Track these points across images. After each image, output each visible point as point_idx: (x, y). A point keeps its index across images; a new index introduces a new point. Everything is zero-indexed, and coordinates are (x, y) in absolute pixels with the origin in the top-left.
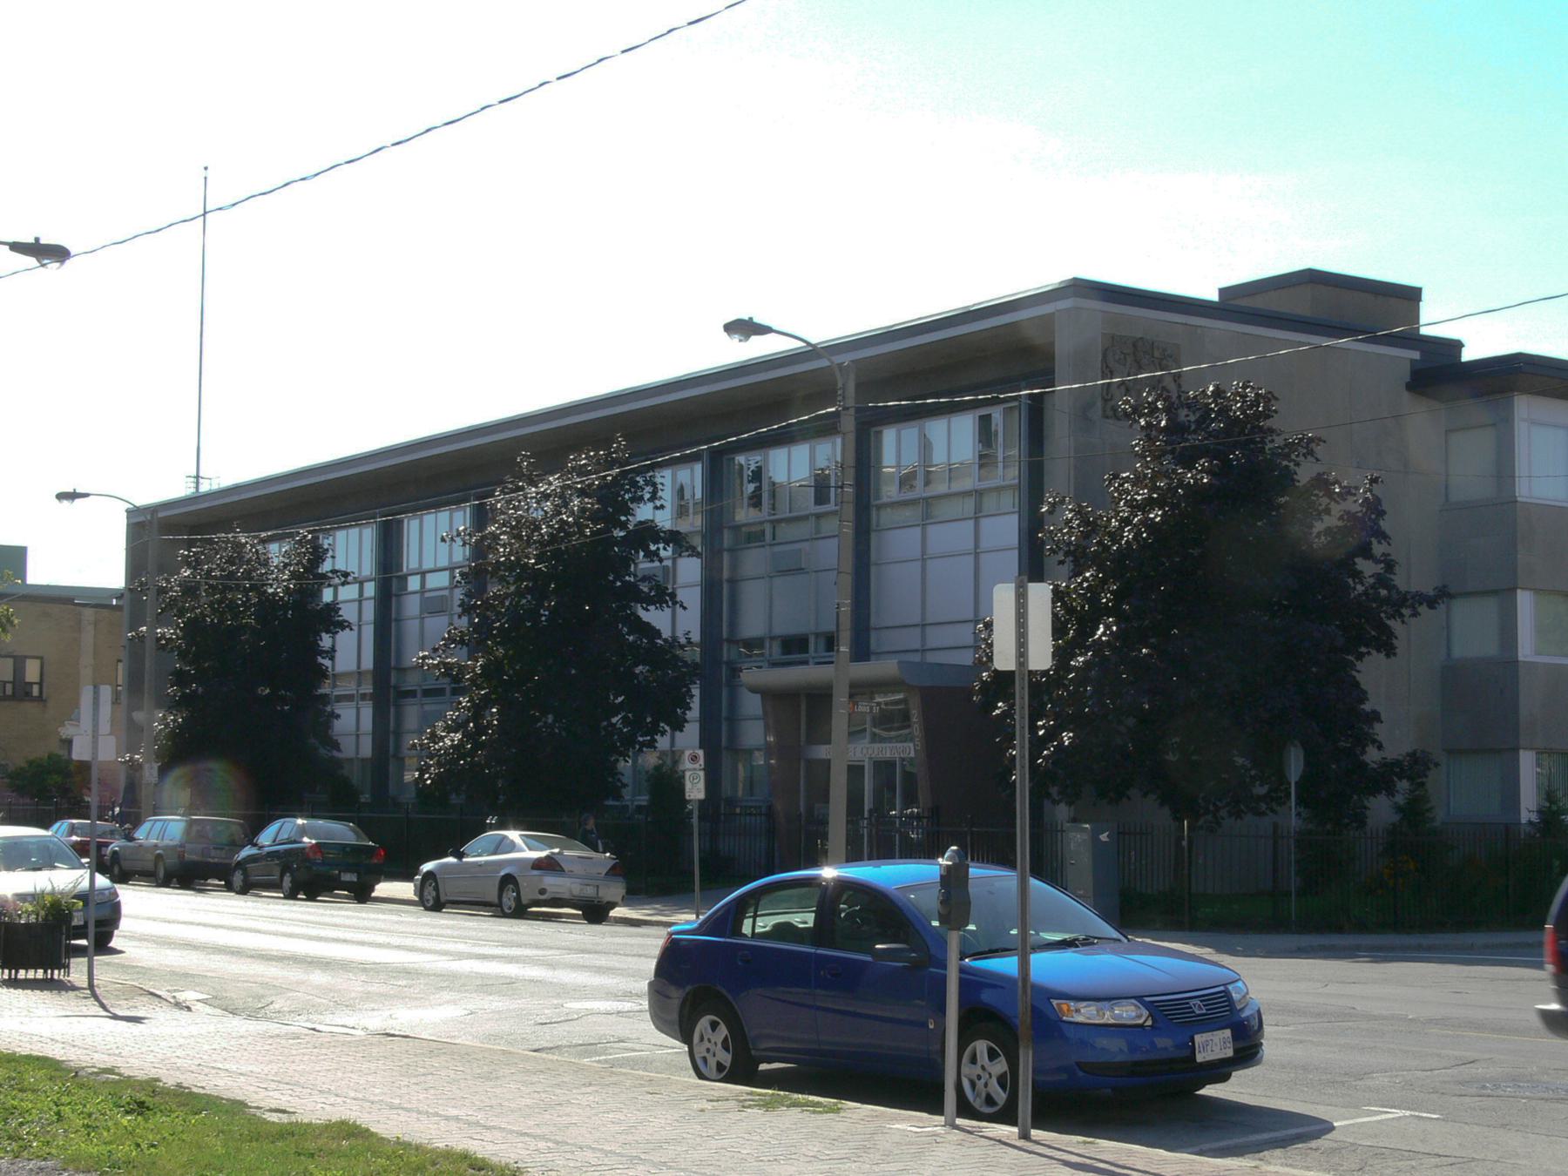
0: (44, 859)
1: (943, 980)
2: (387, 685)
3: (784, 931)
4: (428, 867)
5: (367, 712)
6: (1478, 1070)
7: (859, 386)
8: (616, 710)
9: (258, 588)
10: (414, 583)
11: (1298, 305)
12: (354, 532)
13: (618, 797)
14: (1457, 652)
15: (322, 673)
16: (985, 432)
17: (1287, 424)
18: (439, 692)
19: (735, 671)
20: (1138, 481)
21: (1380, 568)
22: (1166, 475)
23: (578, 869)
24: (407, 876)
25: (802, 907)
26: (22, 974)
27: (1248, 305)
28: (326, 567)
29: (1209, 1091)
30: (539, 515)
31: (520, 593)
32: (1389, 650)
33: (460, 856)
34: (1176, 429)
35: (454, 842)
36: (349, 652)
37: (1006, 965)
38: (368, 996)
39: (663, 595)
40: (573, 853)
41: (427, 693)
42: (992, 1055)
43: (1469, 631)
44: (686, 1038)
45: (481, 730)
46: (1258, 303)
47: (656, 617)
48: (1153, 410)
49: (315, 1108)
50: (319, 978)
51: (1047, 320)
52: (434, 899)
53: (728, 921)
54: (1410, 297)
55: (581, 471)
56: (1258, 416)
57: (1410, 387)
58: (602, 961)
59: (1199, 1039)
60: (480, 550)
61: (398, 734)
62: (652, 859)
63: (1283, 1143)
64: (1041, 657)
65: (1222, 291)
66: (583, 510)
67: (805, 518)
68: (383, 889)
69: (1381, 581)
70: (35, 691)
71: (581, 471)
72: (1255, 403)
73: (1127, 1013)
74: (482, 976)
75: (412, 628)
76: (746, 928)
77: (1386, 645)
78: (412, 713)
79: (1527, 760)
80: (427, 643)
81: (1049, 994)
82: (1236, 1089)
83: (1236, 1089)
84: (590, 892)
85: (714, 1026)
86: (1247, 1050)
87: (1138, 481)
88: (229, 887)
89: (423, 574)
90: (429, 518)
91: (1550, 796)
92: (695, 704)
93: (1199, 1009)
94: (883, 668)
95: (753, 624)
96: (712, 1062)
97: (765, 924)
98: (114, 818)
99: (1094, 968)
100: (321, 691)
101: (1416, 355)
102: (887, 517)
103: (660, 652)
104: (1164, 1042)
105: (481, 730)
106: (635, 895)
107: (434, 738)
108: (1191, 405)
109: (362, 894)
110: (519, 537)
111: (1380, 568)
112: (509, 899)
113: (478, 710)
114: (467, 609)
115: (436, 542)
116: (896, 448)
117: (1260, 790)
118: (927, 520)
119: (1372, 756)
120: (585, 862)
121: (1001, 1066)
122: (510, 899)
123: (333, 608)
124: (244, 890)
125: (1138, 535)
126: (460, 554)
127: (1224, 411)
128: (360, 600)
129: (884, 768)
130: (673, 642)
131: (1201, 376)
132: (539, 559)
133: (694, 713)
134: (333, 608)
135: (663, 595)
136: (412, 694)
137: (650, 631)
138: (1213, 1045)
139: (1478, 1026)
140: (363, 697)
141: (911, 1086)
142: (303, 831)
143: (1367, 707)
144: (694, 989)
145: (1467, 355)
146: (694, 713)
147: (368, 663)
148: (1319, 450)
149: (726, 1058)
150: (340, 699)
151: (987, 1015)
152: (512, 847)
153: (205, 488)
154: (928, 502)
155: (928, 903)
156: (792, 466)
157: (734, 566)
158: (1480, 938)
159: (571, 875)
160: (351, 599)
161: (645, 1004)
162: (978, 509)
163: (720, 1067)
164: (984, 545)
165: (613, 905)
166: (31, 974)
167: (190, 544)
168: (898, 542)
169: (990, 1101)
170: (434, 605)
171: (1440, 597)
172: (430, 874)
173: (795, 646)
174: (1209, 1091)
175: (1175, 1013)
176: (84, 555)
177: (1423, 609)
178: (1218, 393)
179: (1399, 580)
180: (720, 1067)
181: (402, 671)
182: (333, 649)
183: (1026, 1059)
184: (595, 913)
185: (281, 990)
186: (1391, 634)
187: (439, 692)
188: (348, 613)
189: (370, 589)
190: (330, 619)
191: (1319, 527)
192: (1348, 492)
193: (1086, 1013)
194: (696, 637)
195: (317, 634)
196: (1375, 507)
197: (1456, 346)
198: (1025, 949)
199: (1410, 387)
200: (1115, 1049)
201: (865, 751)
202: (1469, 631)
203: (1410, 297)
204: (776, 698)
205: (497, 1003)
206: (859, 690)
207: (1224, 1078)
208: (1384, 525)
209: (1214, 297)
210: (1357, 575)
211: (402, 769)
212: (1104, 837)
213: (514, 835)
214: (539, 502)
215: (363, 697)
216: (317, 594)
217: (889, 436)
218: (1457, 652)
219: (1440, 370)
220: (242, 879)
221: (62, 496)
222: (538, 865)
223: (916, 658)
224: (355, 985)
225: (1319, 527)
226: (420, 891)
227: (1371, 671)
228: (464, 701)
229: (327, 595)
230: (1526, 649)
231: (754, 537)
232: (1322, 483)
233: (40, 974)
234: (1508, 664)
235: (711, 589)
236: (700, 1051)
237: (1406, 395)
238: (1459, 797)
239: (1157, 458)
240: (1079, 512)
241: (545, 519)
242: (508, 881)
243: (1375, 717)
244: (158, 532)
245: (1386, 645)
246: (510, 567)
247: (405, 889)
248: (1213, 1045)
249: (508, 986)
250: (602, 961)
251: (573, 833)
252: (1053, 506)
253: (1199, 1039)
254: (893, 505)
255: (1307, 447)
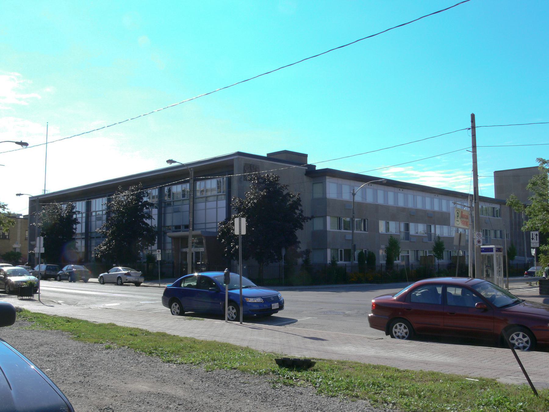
0: (22, 274)
1: (225, 295)
2: (88, 236)
3: (189, 286)
4: (101, 275)
5: (83, 242)
6: (323, 310)
7: (195, 173)
8: (140, 241)
9: (60, 215)
10: (94, 214)
11: (283, 157)
12: (81, 202)
13: (140, 260)
14: (315, 229)
15: (74, 233)
16: (218, 183)
17: (282, 182)
18: (99, 237)
19: (165, 233)
20: (251, 194)
21: (300, 212)
22: (257, 193)
23: (134, 275)
24: (97, 278)
25: (193, 281)
26: (24, 298)
27: (273, 157)
28: (74, 210)
29: (274, 315)
30: (123, 199)
31: (119, 216)
32: (302, 229)
33: (108, 272)
34: (259, 183)
35: (107, 269)
36: (80, 229)
37: (237, 291)
38: (98, 301)
39: (150, 217)
40: (133, 272)
41: (97, 238)
42: (233, 309)
43: (317, 224)
44: (170, 307)
45: (111, 246)
46: (275, 157)
47: (148, 221)
48: (254, 179)
49: (107, 322)
50: (85, 298)
51: (233, 160)
52: (103, 282)
53: (179, 284)
54: (306, 156)
55: (133, 191)
56: (276, 181)
57: (306, 175)
58: (144, 294)
59: (272, 305)
60: (109, 207)
61: (90, 246)
62: (150, 273)
63: (289, 324)
64: (244, 232)
65: (268, 154)
66: (133, 198)
67: (180, 200)
68: (90, 280)
69: (300, 214)
70: (7, 237)
71: (133, 191)
72: (275, 178)
73: (259, 300)
74: (120, 297)
75: (93, 223)
76: (182, 285)
77: (301, 227)
78: (93, 242)
79: (329, 251)
80: (98, 227)
81: (244, 297)
82: (279, 314)
83: (279, 314)
84: (137, 280)
85: (176, 305)
86: (281, 307)
87: (251, 194)
88: (56, 280)
89: (96, 212)
90: (97, 200)
91: (333, 258)
92: (157, 240)
93: (272, 299)
94: (198, 232)
95: (169, 223)
96: (176, 312)
97: (186, 284)
98: (26, 265)
99: (253, 293)
100: (74, 237)
101: (307, 168)
102: (197, 200)
103: (149, 229)
104: (266, 306)
105: (111, 246)
106: (146, 280)
107: (100, 247)
108: (262, 178)
109: (86, 281)
110: (118, 204)
111: (300, 212)
112: (119, 282)
113: (109, 241)
114: (107, 220)
115: (99, 205)
116: (200, 185)
117: (276, 257)
118: (206, 201)
119: (298, 250)
120: (135, 274)
121: (235, 311)
122: (119, 281)
123: (76, 219)
124: (60, 280)
125: (251, 205)
126: (105, 207)
127: (269, 180)
128: (82, 217)
129: (197, 253)
130: (152, 227)
131: (264, 173)
132: (123, 209)
133: (156, 242)
134: (76, 219)
135: (150, 217)
136: (94, 238)
137: (147, 224)
138: (275, 306)
139: (322, 302)
140: (83, 238)
141: (220, 316)
142: (73, 267)
143: (298, 240)
144: (172, 299)
145: (317, 168)
146: (156, 242)
147: (84, 231)
148: (288, 187)
149: (178, 311)
150: (77, 239)
151: (235, 302)
152: (120, 270)
153: (46, 193)
154: (207, 197)
155: (222, 280)
156: (177, 189)
157: (165, 210)
158: (318, 287)
159: (133, 276)
160: (80, 217)
161: (161, 302)
162: (217, 199)
163: (177, 313)
164: (218, 206)
165: (141, 283)
166: (26, 298)
167: (44, 205)
168: (201, 206)
169: (232, 318)
170: (99, 219)
171: (312, 217)
172: (102, 276)
173: (178, 228)
174: (274, 315)
175: (268, 300)
176: (21, 208)
177: (309, 220)
178: (268, 176)
179: (303, 214)
180: (177, 313)
181: (91, 233)
182: (76, 228)
183: (241, 309)
184: (137, 284)
185: (79, 300)
186: (302, 225)
187: (99, 237)
188: (79, 220)
189: (84, 215)
190: (75, 221)
191: (288, 203)
192: (294, 196)
193: (251, 300)
194: (157, 226)
195: (73, 225)
196: (299, 200)
197: (315, 166)
198: (241, 288)
199: (306, 175)
200: (257, 307)
201: (194, 250)
202: (317, 224)
203: (306, 156)
204: (174, 238)
205: (125, 302)
206: (194, 236)
207: (277, 312)
208: (301, 203)
209: (266, 155)
210: (296, 213)
211: (91, 254)
212: (245, 267)
213: (120, 268)
214: (123, 197)
215: (83, 238)
216: (72, 216)
217: (198, 183)
218: (315, 229)
219: (311, 171)
220: (61, 278)
221: (17, 195)
222: (125, 274)
223: (204, 230)
224: (94, 299)
225: (288, 203)
226: (100, 280)
227: (299, 233)
228: (107, 239)
229: (74, 216)
230: (329, 228)
231: (169, 204)
232: (288, 194)
233: (28, 298)
234: (325, 231)
235: (160, 214)
236: (173, 310)
237: (305, 177)
238: (315, 258)
239: (255, 189)
240: (239, 200)
241: (125, 201)
242: (119, 278)
243: (299, 242)
244: (37, 203)
245: (301, 227)
246: (117, 211)
247: (96, 280)
248: (275, 306)
249: (127, 299)
250: (144, 294)
251: (134, 268)
252: (234, 199)
253: (272, 305)
254: (199, 198)
255: (286, 186)
